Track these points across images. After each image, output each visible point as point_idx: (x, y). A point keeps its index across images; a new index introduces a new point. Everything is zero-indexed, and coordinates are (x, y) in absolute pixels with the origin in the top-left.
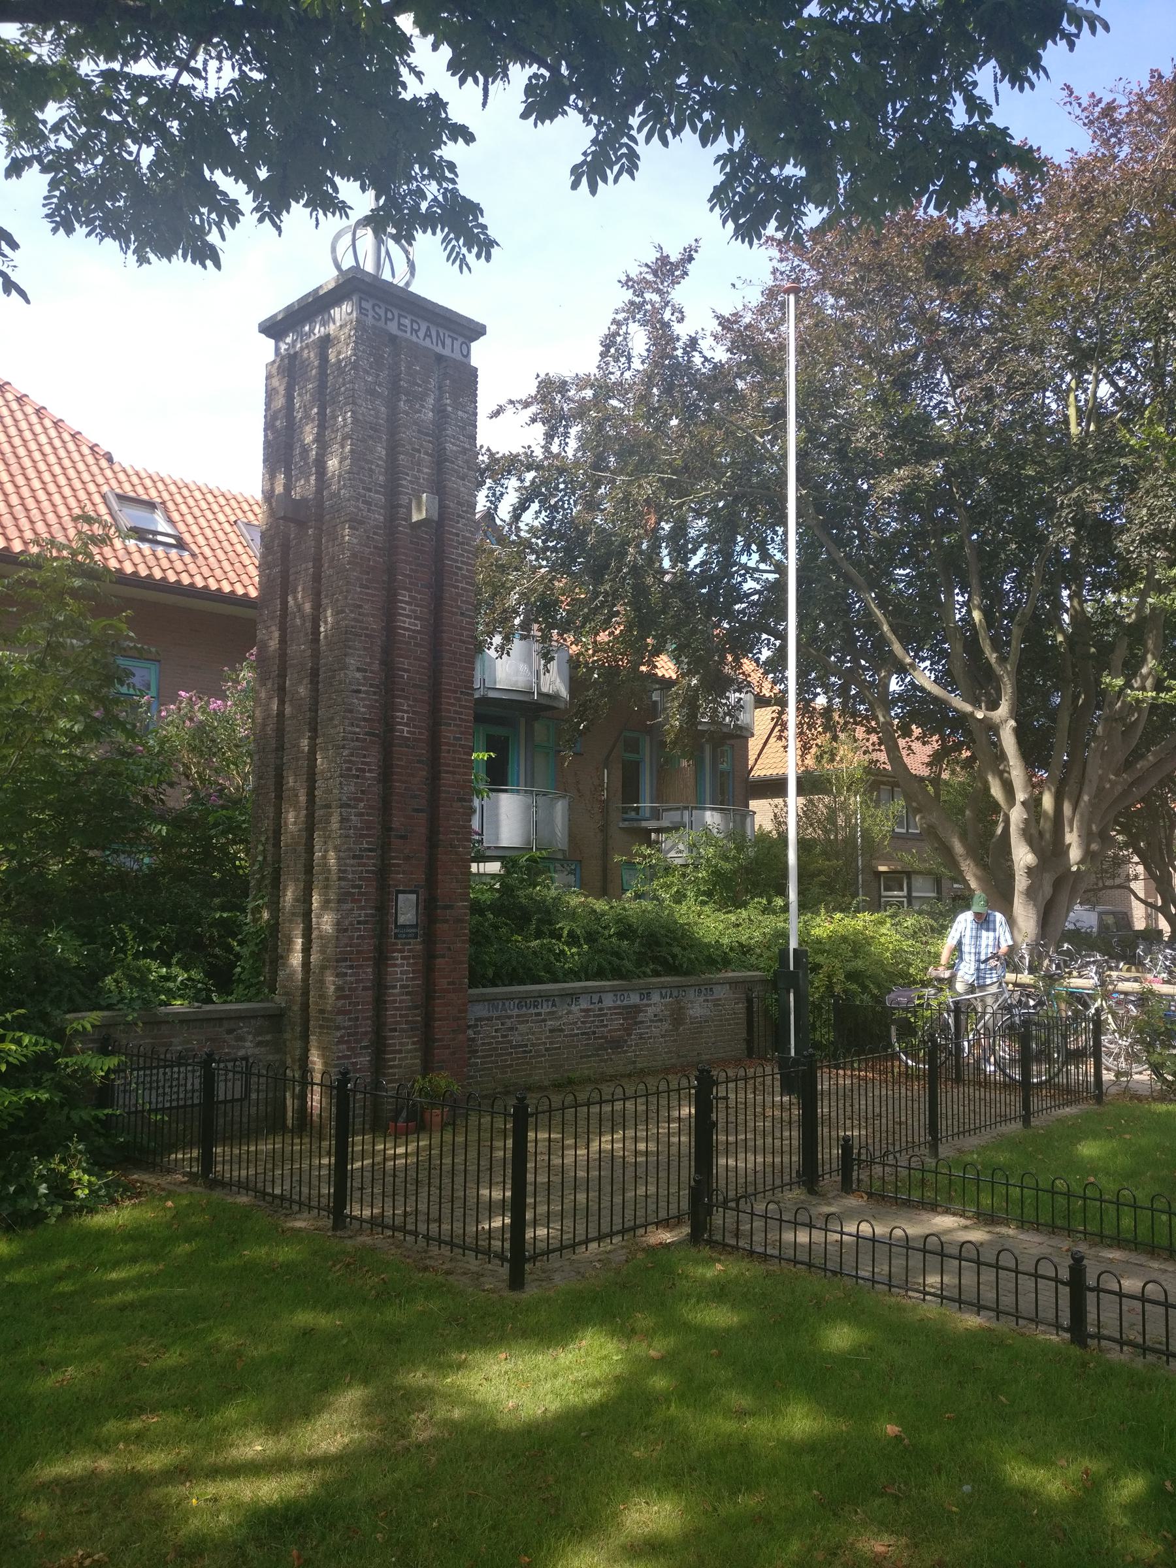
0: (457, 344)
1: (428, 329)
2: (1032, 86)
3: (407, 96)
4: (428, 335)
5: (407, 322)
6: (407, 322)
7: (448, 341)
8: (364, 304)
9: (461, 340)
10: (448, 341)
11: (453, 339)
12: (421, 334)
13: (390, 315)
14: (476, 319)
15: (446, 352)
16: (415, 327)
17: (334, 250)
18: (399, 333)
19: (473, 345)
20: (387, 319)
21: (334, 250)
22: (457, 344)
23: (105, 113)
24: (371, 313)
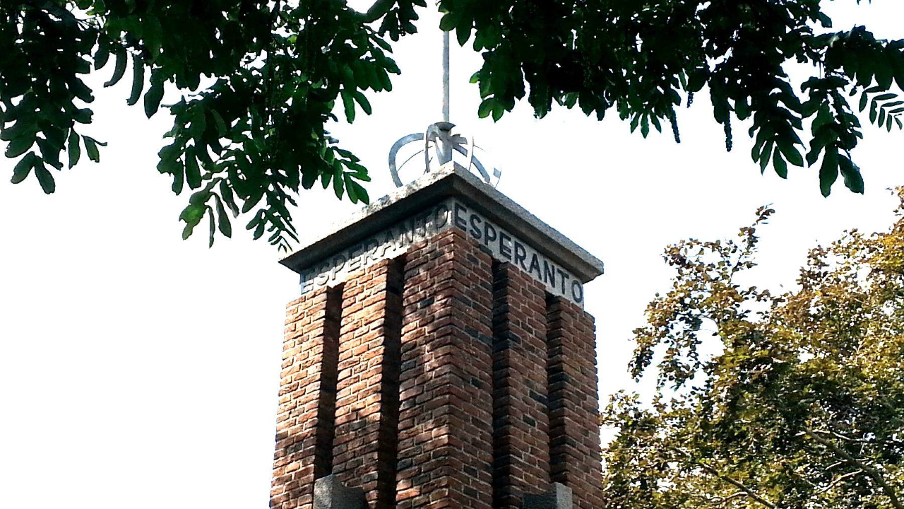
0: (568, 283)
1: (535, 258)
2: (368, 109)
3: (202, 76)
4: (534, 265)
5: (510, 244)
6: (510, 244)
7: (558, 278)
8: (461, 214)
9: (572, 278)
10: (558, 278)
11: (564, 276)
12: (527, 263)
13: (491, 234)
14: (593, 253)
15: (556, 292)
16: (520, 253)
17: (392, 161)
18: (503, 259)
19: (586, 287)
20: (487, 238)
21: (392, 161)
22: (568, 283)
23: (79, 54)
24: (469, 226)
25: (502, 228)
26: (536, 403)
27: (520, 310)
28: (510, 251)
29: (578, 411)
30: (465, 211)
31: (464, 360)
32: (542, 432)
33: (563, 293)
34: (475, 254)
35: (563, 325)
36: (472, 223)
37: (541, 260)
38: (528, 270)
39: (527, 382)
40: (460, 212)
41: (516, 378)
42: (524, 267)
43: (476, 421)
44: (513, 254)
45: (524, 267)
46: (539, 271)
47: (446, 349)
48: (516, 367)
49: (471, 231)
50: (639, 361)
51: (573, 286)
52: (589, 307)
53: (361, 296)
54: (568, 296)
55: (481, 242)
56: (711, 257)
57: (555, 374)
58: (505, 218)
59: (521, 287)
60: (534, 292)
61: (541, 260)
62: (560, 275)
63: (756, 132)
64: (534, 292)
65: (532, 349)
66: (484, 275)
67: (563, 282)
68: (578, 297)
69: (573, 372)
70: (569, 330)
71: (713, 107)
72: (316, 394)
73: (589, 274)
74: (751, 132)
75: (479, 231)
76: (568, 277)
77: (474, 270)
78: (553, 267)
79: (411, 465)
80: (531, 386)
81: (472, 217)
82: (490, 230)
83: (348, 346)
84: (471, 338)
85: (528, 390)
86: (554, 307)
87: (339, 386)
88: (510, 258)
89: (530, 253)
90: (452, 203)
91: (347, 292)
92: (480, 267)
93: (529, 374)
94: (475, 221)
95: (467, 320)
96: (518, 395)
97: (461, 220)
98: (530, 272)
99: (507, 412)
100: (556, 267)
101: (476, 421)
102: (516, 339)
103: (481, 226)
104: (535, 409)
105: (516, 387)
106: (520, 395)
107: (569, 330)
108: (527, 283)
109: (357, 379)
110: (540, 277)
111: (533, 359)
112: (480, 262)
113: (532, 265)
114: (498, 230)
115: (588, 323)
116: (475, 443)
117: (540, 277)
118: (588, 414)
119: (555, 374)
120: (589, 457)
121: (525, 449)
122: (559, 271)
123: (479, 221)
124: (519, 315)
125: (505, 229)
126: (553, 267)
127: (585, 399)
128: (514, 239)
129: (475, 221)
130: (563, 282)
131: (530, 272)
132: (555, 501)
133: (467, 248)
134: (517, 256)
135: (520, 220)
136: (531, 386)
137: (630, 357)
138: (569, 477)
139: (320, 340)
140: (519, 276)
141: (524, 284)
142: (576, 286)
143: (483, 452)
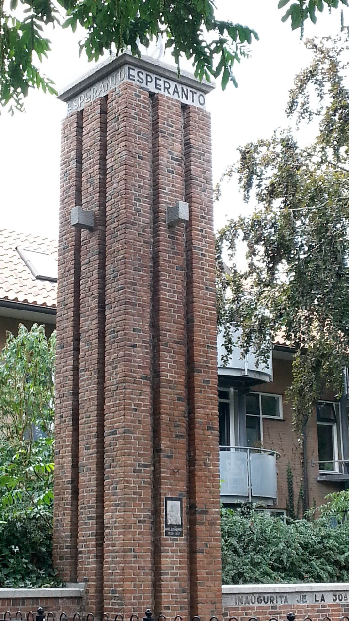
4: (176, 90)
7: (190, 95)
8: (132, 72)
9: (199, 93)
10: (190, 95)
12: (171, 90)
15: (188, 102)
18: (156, 91)
19: (207, 96)
24: (136, 78)
25: (156, 74)
26: (175, 162)
27: (166, 117)
28: (161, 86)
29: (200, 163)
30: (134, 70)
31: (133, 147)
32: (178, 176)
33: (193, 101)
34: (139, 92)
35: (191, 119)
36: (138, 75)
37: (179, 87)
38: (172, 94)
39: (170, 153)
40: (131, 71)
41: (163, 152)
42: (169, 93)
43: (140, 176)
44: (162, 88)
45: (169, 93)
46: (178, 93)
47: (123, 143)
48: (163, 146)
49: (138, 80)
50: (291, 108)
51: (199, 97)
52: (207, 108)
53: (90, 116)
54: (196, 104)
55: (144, 85)
56: (328, 45)
57: (187, 145)
58: (156, 70)
59: (166, 104)
60: (174, 105)
61: (179, 87)
62: (191, 93)
63: (196, 63)
64: (174, 105)
65: (173, 136)
66: (144, 102)
67: (193, 96)
68: (202, 102)
69: (197, 143)
70: (195, 122)
71: (174, 57)
72: (74, 166)
73: (207, 89)
74: (194, 65)
75: (142, 79)
76: (196, 93)
77: (139, 101)
78: (187, 90)
79: (111, 199)
80: (172, 154)
81: (138, 73)
82: (149, 77)
83: (87, 142)
84: (137, 136)
85: (170, 156)
86: (187, 111)
87: (83, 161)
88: (160, 89)
89: (173, 84)
90: (126, 67)
91: (85, 114)
92: (142, 99)
93: (171, 149)
94: (140, 74)
95: (135, 127)
96: (164, 159)
97: (132, 75)
98: (173, 94)
99: (158, 169)
100: (189, 89)
101: (140, 176)
102: (163, 132)
103: (143, 77)
104: (174, 165)
105: (163, 155)
106: (166, 160)
107: (195, 122)
108: (170, 101)
109: (90, 158)
110: (179, 97)
111: (173, 140)
112: (142, 96)
113: (174, 91)
114: (154, 76)
115: (206, 117)
116: (140, 186)
117: (179, 97)
118: (205, 163)
119: (187, 145)
120: (205, 184)
121: (168, 185)
122: (190, 91)
123: (142, 74)
124: (165, 119)
125: (158, 75)
126: (187, 90)
127: (204, 156)
128: (163, 79)
129: (140, 74)
130: (193, 96)
131: (173, 94)
132: (178, 210)
133: (134, 90)
134: (165, 88)
135: (165, 70)
136: (172, 154)
137: (286, 106)
138: (193, 196)
139: (75, 138)
140: (165, 99)
141: (168, 103)
142: (201, 97)
143: (144, 190)
